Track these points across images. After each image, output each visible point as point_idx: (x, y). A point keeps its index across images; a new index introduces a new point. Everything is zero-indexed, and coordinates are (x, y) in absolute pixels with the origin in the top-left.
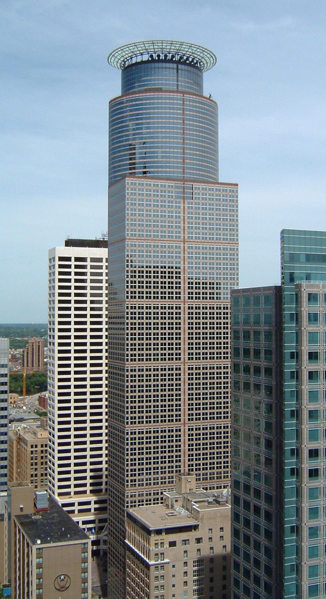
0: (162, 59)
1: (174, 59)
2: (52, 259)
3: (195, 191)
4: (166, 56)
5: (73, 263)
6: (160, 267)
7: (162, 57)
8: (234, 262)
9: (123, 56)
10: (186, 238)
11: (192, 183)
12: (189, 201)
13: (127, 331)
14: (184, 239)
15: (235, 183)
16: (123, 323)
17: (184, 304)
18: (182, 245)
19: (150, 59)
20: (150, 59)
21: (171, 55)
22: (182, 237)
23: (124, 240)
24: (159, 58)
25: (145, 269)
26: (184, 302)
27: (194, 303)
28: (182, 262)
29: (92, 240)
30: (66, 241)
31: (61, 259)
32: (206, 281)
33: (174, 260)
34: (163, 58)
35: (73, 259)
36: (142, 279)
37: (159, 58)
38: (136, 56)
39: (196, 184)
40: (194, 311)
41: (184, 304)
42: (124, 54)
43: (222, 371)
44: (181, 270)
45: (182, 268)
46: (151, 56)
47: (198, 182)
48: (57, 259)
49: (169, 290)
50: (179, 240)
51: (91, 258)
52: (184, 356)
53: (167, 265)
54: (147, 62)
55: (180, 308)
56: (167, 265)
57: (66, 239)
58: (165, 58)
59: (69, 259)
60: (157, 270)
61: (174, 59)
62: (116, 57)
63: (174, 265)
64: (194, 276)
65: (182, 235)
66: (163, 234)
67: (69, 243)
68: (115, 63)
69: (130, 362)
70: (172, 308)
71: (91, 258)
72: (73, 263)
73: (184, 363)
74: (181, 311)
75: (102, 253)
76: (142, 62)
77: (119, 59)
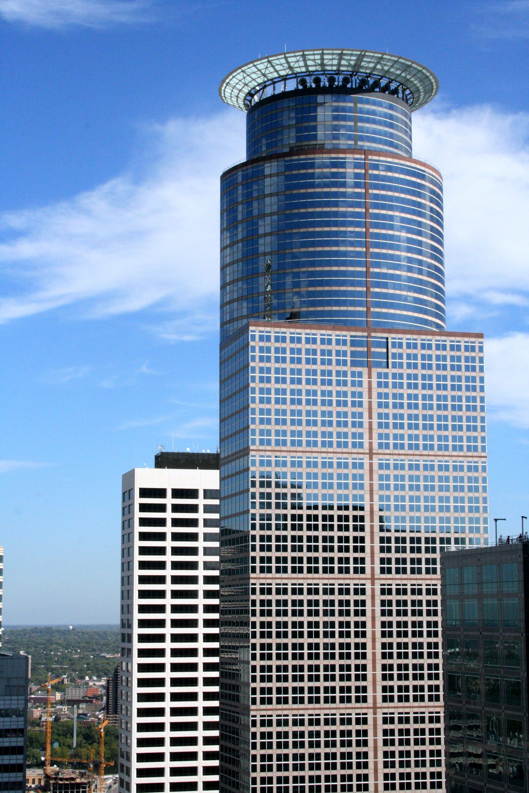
0: (324, 87)
1: (349, 86)
2: (127, 495)
3: (392, 350)
4: (332, 80)
5: (169, 501)
6: (351, 508)
7: (325, 82)
8: (477, 495)
9: (246, 85)
10: (375, 446)
11: (385, 335)
12: (380, 370)
13: (253, 641)
14: (371, 449)
15: (477, 331)
16: (246, 624)
17: (373, 582)
18: (366, 461)
19: (300, 87)
20: (300, 87)
21: (341, 77)
22: (366, 445)
23: (246, 452)
24: (318, 86)
25: (320, 512)
26: (373, 579)
27: (394, 580)
28: (367, 497)
29: (209, 455)
30: (157, 457)
31: (145, 493)
32: (448, 535)
33: (351, 492)
34: (327, 84)
35: (169, 493)
36: (315, 533)
37: (318, 86)
38: (274, 83)
39: (394, 335)
40: (394, 598)
41: (373, 582)
42: (248, 79)
43: (427, 726)
44: (366, 513)
45: (367, 508)
46: (303, 82)
47: (397, 332)
48: (137, 493)
49: (310, 554)
50: (361, 451)
51: (205, 491)
52: (375, 694)
53: (335, 503)
54: (295, 93)
55: (363, 592)
56: (335, 503)
57: (157, 452)
58: (331, 85)
59: (161, 493)
60: (331, 512)
61: (349, 86)
62: (234, 87)
63: (351, 503)
64: (408, 525)
65: (366, 441)
66: (335, 436)
67: (164, 461)
68: (234, 99)
69: (258, 706)
70: (285, 591)
71: (205, 491)
72: (169, 501)
73: (375, 708)
74: (367, 597)
75: (207, 479)
76: (285, 95)
77: (240, 91)
